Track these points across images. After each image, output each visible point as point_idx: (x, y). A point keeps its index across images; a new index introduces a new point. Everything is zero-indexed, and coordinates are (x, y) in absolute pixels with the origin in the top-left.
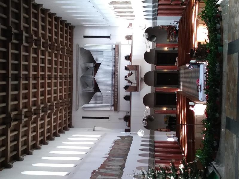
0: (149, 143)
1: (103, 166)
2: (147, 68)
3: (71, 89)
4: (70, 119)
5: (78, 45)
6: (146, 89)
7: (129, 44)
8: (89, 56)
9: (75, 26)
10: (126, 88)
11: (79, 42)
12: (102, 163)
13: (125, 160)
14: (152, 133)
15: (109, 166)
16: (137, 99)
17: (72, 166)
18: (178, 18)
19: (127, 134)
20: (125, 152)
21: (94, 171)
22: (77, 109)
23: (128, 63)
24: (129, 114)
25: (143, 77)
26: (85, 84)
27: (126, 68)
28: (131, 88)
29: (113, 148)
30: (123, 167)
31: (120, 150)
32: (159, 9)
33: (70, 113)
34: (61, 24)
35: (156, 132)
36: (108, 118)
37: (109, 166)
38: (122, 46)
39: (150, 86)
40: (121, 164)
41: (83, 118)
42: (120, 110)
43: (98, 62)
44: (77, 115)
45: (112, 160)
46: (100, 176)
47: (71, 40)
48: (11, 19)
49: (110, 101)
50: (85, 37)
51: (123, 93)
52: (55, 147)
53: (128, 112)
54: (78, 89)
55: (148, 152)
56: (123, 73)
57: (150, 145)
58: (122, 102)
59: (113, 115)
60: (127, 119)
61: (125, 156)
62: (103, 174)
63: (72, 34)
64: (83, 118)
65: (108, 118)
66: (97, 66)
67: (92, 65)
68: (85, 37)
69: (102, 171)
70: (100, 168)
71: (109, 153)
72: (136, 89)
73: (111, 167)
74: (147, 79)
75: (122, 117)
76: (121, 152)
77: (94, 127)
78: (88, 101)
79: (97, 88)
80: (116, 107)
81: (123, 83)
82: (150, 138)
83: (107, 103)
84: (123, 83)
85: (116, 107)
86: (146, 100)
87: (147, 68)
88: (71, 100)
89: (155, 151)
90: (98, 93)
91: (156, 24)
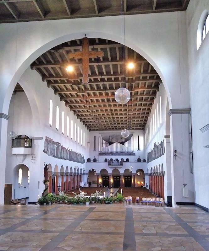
0: (80, 172)
1: (63, 148)
2: (122, 171)
3: (110, 129)
4: (93, 130)
5: (134, 132)
6: (110, 171)
7: (135, 160)
8: (128, 139)
9: (144, 130)
10: (111, 159)
11: (136, 133)
12: (65, 148)
13: (68, 160)
14: (86, 174)
15: (63, 151)
16: (105, 166)
17: (63, 131)
18: (148, 188)
19: (86, 161)
20: (74, 160)
21: (60, 144)
22: (99, 133)
23: (125, 160)
24: (97, 161)
25: (117, 168)
26: (112, 137)
27: (122, 159)
28: (110, 163)
29: (75, 153)
30: (63, 158)
31: (74, 157)
32: (158, 176)
33: (97, 130)
34: (144, 123)
35: (87, 176)
36: (95, 150)
37: (63, 151)
38: (134, 156)
39: (111, 172)
40: (65, 158)
41: (95, 137)
42: (100, 157)
43: (125, 144)
44: (97, 133)
45: (67, 153)
46: (56, 147)
47: (137, 129)
48: (139, 90)
49: (104, 151)
50: (139, 136)
51: (109, 158)
52: (76, 122)
53: (98, 161)
54: (109, 133)
55: (65, 171)
56: (119, 158)
57: (78, 173)
58: (103, 158)
59: (97, 153)
60: (95, 161)
61: (70, 159)
62: (58, 149)
63: (140, 129)
64: (95, 137)
65: (95, 150)
66: (123, 143)
67: (123, 140)
68: (139, 136)
69: (60, 148)
70: (62, 147)
71: (72, 151)
72: (110, 165)
73: (63, 152)
74: (116, 170)
75: (140, 158)
76: (73, 157)
77: (90, 143)
78: (103, 139)
79: (110, 143)
80: (101, 154)
81: (114, 158)
82: (70, 173)
83: (103, 149)
84: (114, 158)
85: (101, 154)
86: (104, 170)
87: (122, 171)
88: (104, 130)
89: (74, 176)
90: (108, 144)
91: (87, 173)
